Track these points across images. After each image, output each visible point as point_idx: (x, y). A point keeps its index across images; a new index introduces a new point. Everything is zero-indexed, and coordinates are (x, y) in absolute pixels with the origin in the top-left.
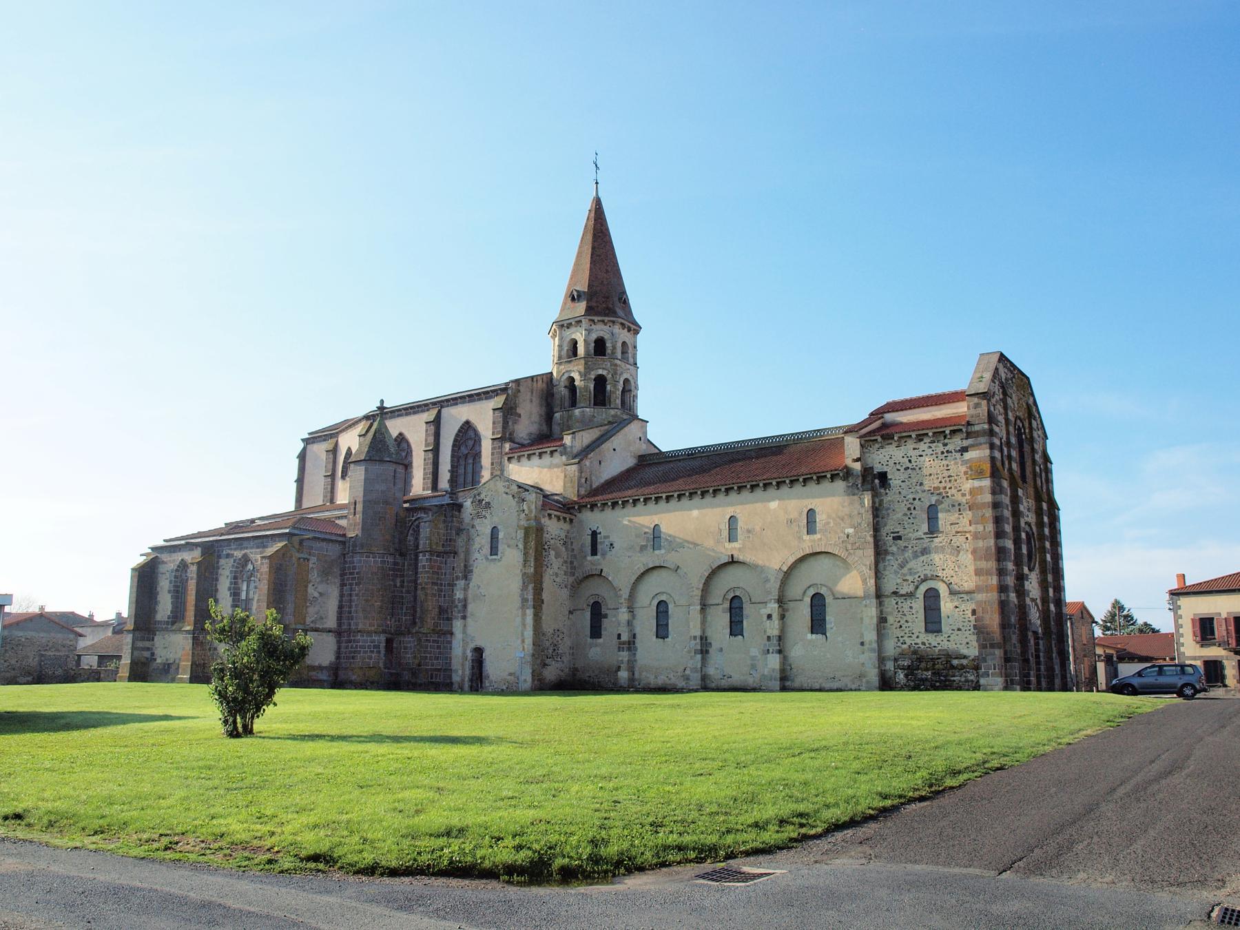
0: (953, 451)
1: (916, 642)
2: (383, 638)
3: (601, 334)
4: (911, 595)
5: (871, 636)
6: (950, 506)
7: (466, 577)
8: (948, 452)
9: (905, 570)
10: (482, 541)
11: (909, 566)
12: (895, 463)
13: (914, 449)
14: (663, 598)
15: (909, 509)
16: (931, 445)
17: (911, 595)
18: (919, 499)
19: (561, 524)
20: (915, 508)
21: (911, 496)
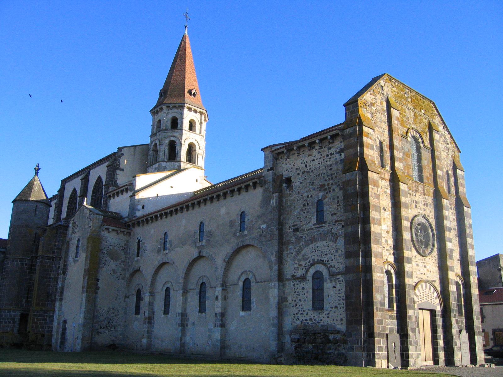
0: (335, 153)
1: (306, 318)
2: (18, 314)
3: (174, 115)
4: (303, 278)
5: (274, 313)
6: (332, 200)
7: (64, 273)
8: (331, 154)
9: (300, 257)
10: (73, 249)
11: (303, 253)
12: (297, 169)
13: (309, 156)
14: (168, 285)
15: (304, 205)
16: (320, 150)
17: (303, 278)
18: (311, 196)
19: (121, 236)
20: (308, 204)
21: (306, 194)
